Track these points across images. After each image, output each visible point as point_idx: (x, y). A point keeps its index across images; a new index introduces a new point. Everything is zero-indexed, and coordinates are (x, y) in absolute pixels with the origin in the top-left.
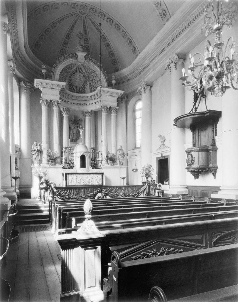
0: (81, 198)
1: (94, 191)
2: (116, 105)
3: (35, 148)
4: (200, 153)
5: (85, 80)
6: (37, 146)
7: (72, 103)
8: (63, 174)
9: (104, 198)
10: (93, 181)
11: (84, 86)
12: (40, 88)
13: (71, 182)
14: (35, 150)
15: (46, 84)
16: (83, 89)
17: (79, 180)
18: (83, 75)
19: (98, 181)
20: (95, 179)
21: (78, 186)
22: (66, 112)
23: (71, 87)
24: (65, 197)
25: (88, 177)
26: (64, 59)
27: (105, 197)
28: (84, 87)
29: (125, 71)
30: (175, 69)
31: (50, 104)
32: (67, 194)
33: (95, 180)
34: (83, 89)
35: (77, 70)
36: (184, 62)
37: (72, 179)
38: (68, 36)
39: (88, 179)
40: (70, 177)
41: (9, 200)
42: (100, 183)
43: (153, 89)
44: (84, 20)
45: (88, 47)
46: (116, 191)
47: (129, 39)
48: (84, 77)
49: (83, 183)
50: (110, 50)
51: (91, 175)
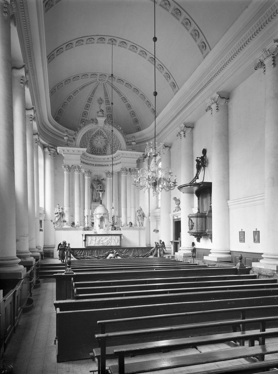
0: (94, 258)
1: (106, 252)
2: (136, 166)
3: (57, 211)
4: (199, 219)
5: (107, 142)
6: (59, 209)
7: (93, 165)
8: (83, 235)
9: (115, 258)
10: (112, 242)
11: (105, 148)
12: (62, 154)
13: (90, 243)
14: (57, 213)
15: (68, 151)
16: (104, 150)
17: (97, 241)
18: (104, 137)
19: (117, 242)
20: (114, 240)
21: (96, 247)
22: (87, 174)
23: (93, 149)
24: (80, 257)
25: (106, 238)
26: (85, 125)
27: (116, 257)
28: (105, 148)
29: (147, 132)
30: (273, 66)
31: (70, 169)
32: (82, 255)
33: (114, 242)
34: (104, 150)
35: (97, 133)
36: (227, 102)
37: (92, 240)
38: (90, 100)
39: (107, 240)
40: (89, 238)
41: (34, 258)
42: (118, 244)
43: (172, 150)
44: (104, 85)
45: (109, 108)
46: (126, 252)
47: (148, 102)
48: (105, 139)
49: (102, 244)
50: (131, 110)
51: (110, 237)
